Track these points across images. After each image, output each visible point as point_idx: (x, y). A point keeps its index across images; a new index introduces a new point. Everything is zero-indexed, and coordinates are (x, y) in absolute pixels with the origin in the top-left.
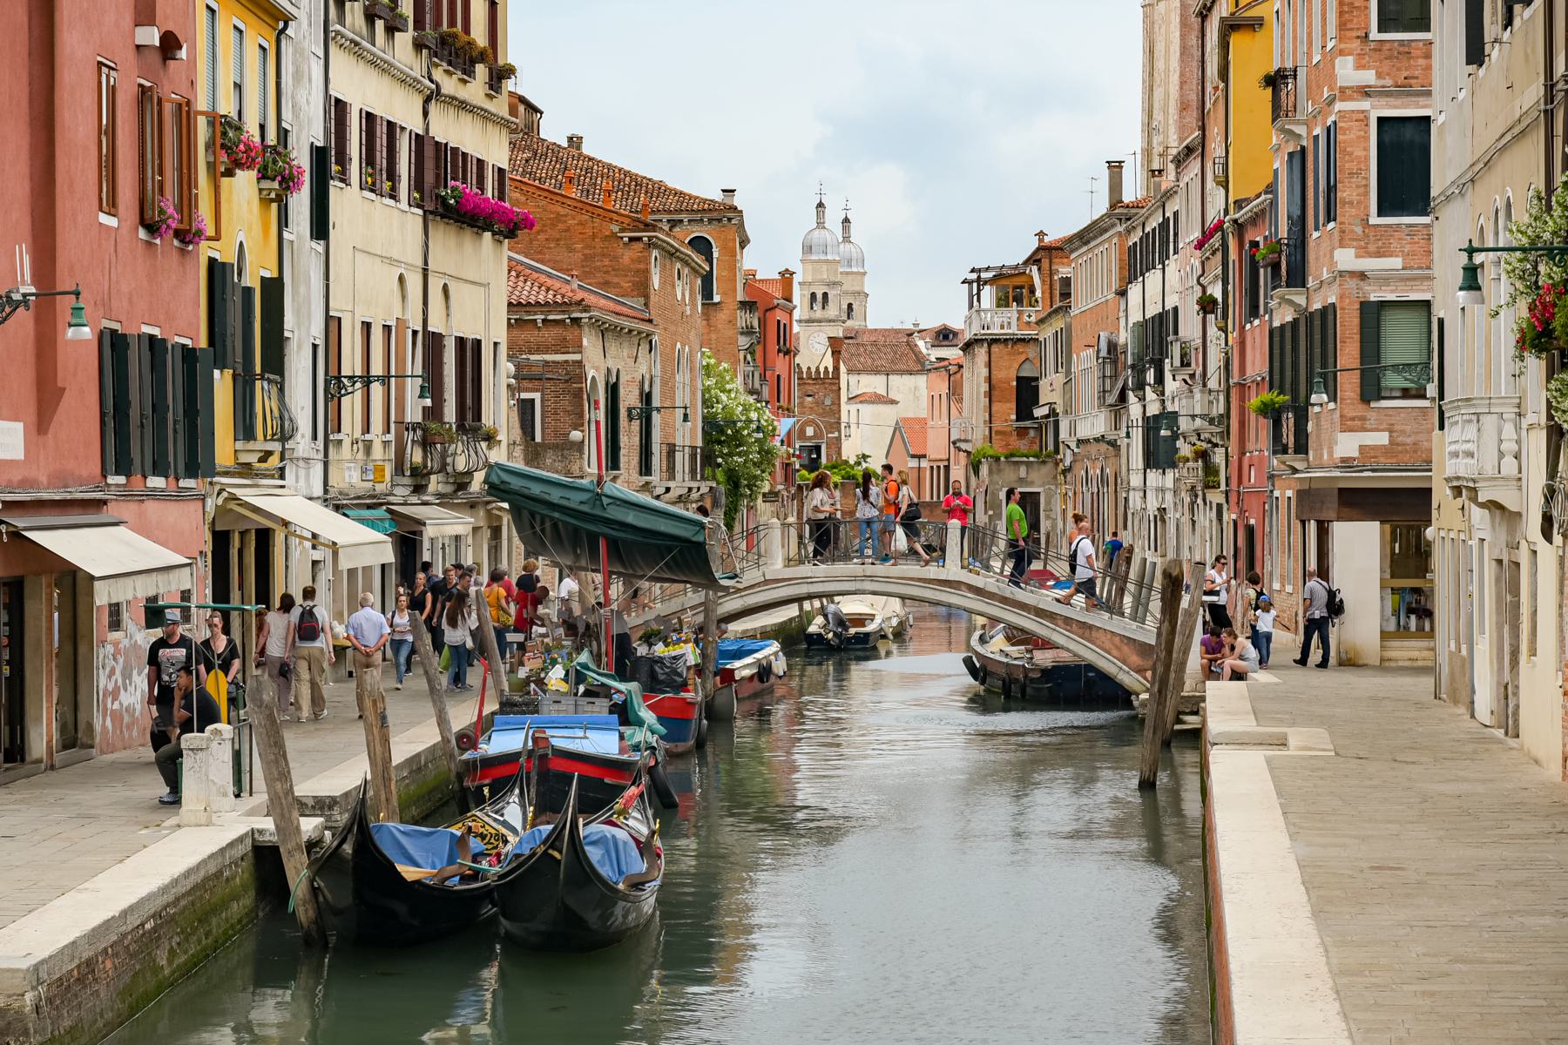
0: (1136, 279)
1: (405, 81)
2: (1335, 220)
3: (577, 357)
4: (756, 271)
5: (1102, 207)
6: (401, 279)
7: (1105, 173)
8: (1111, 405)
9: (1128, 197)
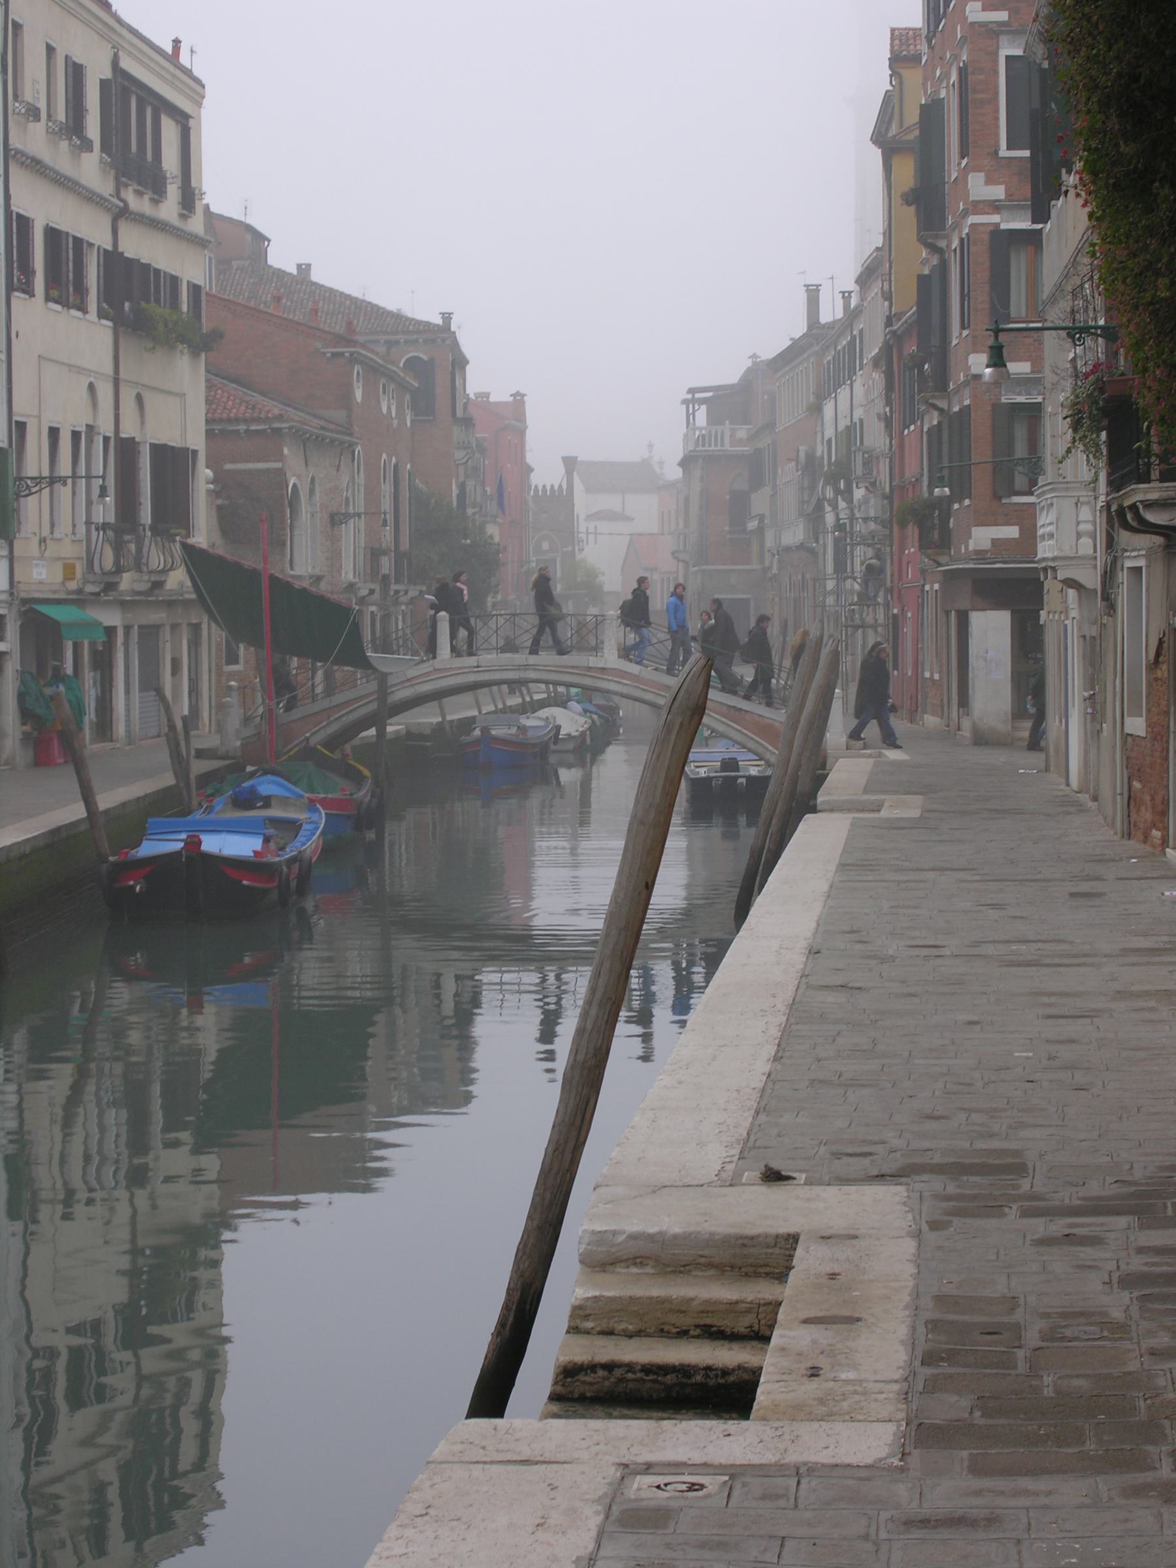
0: (830, 394)
1: (91, 198)
2: (969, 326)
3: (278, 465)
4: (489, 394)
5: (799, 328)
6: (91, 387)
7: (802, 297)
8: (808, 514)
9: (825, 317)
